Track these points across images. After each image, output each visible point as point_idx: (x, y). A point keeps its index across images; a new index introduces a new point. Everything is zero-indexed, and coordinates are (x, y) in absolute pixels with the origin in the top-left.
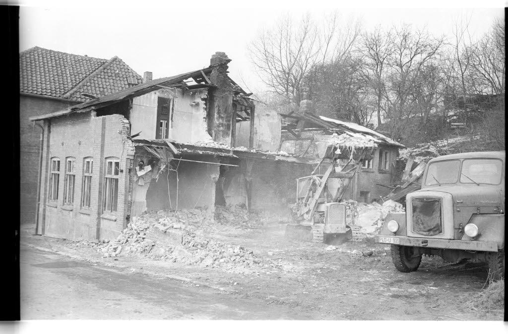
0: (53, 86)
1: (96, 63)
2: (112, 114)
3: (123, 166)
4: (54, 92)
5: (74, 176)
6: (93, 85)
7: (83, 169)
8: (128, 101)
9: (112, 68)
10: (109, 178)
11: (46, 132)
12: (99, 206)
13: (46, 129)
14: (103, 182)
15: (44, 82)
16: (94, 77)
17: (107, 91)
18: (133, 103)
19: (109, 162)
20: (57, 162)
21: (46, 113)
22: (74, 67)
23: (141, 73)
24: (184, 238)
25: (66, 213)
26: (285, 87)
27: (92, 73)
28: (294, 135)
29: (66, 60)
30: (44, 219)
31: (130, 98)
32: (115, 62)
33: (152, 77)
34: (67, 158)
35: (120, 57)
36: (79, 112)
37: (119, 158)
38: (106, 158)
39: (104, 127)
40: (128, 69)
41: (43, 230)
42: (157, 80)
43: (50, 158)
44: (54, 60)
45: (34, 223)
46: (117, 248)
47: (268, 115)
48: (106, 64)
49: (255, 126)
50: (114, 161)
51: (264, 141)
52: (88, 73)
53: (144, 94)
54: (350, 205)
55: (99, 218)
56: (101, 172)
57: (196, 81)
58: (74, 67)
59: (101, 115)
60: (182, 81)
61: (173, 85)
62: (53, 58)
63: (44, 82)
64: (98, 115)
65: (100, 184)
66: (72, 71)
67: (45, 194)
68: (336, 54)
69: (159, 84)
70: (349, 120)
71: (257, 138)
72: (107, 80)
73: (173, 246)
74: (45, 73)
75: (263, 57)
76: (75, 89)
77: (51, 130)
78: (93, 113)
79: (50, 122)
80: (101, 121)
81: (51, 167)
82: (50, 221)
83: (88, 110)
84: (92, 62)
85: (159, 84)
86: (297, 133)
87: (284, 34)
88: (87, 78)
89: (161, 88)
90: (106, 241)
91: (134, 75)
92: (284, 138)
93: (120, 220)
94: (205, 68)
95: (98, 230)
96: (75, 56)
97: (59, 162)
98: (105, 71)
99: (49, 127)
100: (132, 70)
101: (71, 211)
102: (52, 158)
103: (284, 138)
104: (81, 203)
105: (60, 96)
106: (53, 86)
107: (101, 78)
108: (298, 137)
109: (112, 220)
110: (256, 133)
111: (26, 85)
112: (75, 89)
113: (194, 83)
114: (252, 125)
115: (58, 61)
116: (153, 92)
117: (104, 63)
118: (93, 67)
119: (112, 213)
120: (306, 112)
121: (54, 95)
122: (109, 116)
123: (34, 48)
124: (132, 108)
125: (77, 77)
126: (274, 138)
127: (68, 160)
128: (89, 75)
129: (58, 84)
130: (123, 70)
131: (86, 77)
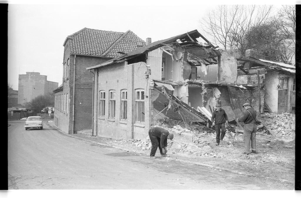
0: (96, 50)
1: (118, 35)
2: (138, 62)
3: (147, 93)
4: (97, 53)
5: (115, 101)
6: (118, 48)
7: (121, 97)
8: (145, 54)
9: (127, 37)
10: (138, 102)
11: (96, 76)
12: (133, 119)
13: (96, 74)
14: (134, 103)
15: (91, 48)
16: (118, 43)
17: (126, 51)
18: (148, 56)
19: (123, 92)
20: (103, 93)
21: (93, 66)
22: (106, 38)
23: (144, 39)
24: (194, 138)
25: (110, 123)
26: (224, 44)
27: (116, 41)
28: (244, 71)
29: (101, 34)
30: (97, 126)
31: (147, 52)
32: (129, 34)
33: (151, 41)
34: (109, 90)
35: (131, 30)
36: (118, 62)
37: (144, 89)
38: (135, 89)
39: (133, 71)
40: (137, 37)
41: (97, 133)
42: (154, 42)
43: (99, 91)
44: (95, 35)
45: (91, 129)
46: (148, 144)
47: (229, 59)
48: (124, 35)
49: (221, 67)
50: (140, 91)
51: (227, 76)
52: (114, 41)
53: (154, 50)
54: (287, 116)
55: (133, 126)
56: (133, 98)
57: (182, 41)
58: (106, 38)
59: (132, 64)
60: (176, 40)
61: (171, 43)
62: (95, 33)
63: (91, 48)
64: (128, 64)
65: (133, 105)
66: (105, 40)
67: (97, 112)
68: (257, 21)
69: (163, 43)
70: (278, 61)
71: (222, 75)
72: (125, 44)
73: (187, 144)
74: (91, 43)
75: (208, 26)
76: (108, 51)
77: (99, 75)
78: (126, 63)
79: (98, 70)
80: (131, 66)
81: (135, 97)
82: (101, 128)
83: (123, 61)
84: (116, 35)
85: (163, 43)
86: (246, 71)
87: (223, 11)
88: (114, 44)
89: (164, 45)
90: (139, 140)
91: (140, 40)
92: (239, 74)
93: (148, 127)
94: (189, 32)
95: (133, 133)
96: (106, 32)
97: (104, 93)
98: (124, 39)
99: (98, 73)
100: (138, 37)
101: (114, 122)
102: (100, 91)
103: (239, 74)
104: (120, 117)
105: (100, 55)
106: (96, 50)
107: (133, 44)
108: (247, 73)
109: (142, 127)
110: (222, 71)
111: (82, 50)
112: (108, 51)
113: (180, 42)
114: (219, 66)
115: (97, 35)
116: (159, 48)
117: (122, 35)
118: (116, 37)
119: (141, 123)
120: (250, 57)
121: (97, 54)
122: (136, 63)
123: (84, 28)
124: (147, 58)
125: (109, 43)
126: (233, 74)
127: (111, 91)
128: (115, 42)
129: (98, 48)
130: (134, 38)
131: (113, 43)
